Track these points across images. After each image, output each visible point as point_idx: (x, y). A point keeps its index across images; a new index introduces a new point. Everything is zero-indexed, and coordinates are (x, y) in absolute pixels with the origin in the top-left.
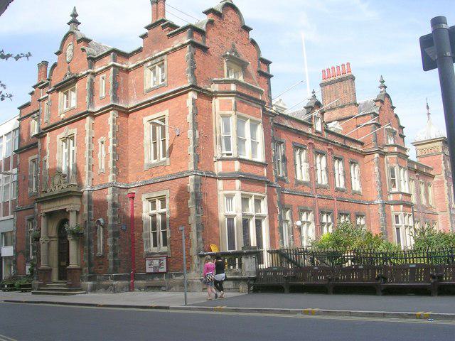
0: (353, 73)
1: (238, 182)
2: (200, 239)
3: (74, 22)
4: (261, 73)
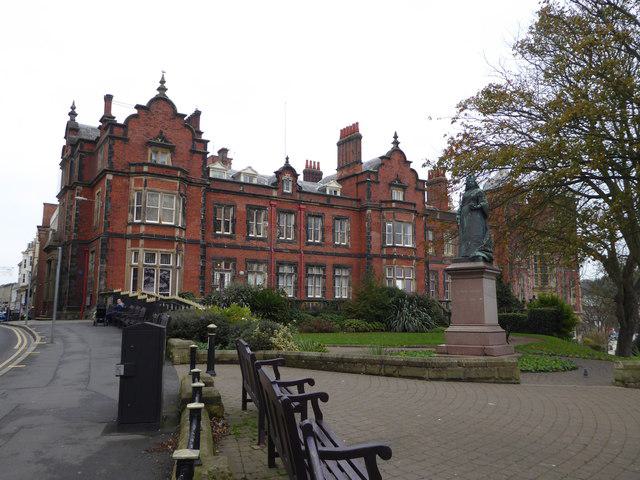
0: (361, 131)
1: (142, 242)
2: (102, 282)
3: (73, 114)
4: (193, 152)
